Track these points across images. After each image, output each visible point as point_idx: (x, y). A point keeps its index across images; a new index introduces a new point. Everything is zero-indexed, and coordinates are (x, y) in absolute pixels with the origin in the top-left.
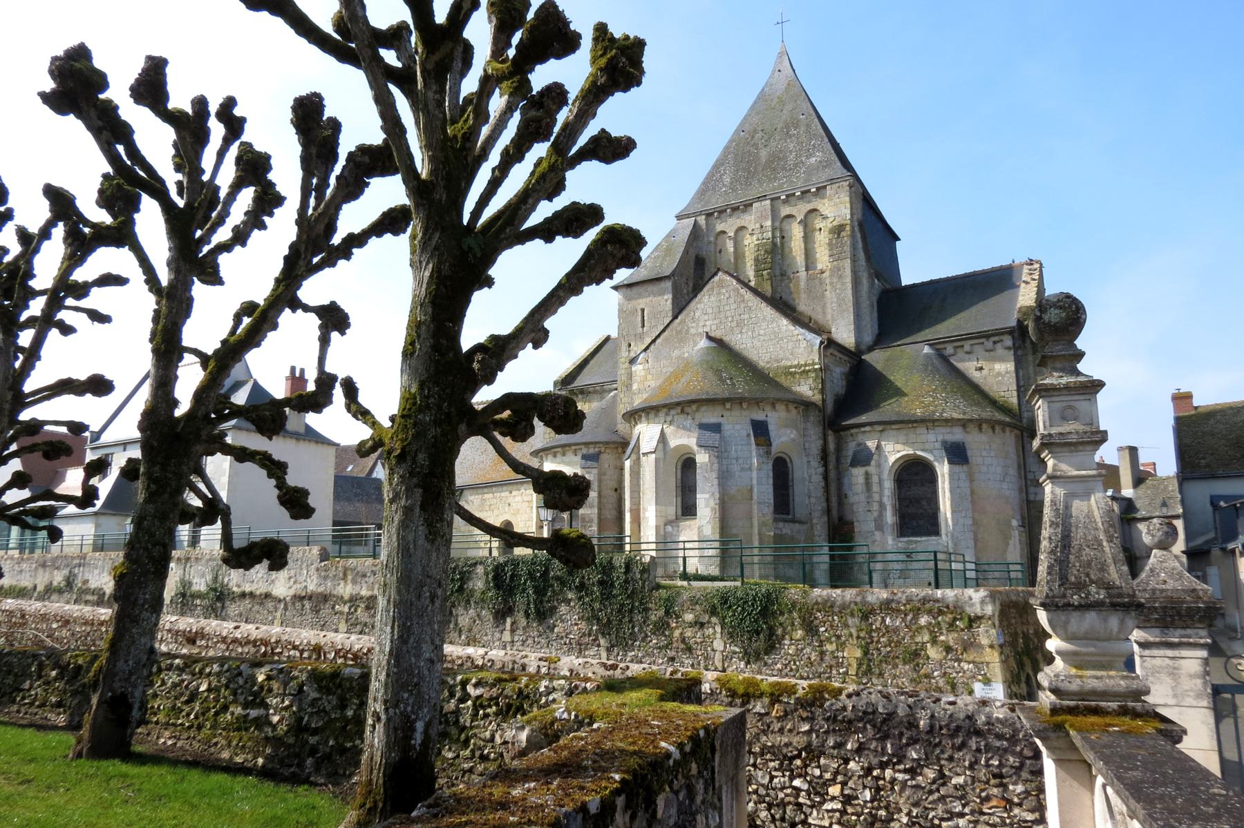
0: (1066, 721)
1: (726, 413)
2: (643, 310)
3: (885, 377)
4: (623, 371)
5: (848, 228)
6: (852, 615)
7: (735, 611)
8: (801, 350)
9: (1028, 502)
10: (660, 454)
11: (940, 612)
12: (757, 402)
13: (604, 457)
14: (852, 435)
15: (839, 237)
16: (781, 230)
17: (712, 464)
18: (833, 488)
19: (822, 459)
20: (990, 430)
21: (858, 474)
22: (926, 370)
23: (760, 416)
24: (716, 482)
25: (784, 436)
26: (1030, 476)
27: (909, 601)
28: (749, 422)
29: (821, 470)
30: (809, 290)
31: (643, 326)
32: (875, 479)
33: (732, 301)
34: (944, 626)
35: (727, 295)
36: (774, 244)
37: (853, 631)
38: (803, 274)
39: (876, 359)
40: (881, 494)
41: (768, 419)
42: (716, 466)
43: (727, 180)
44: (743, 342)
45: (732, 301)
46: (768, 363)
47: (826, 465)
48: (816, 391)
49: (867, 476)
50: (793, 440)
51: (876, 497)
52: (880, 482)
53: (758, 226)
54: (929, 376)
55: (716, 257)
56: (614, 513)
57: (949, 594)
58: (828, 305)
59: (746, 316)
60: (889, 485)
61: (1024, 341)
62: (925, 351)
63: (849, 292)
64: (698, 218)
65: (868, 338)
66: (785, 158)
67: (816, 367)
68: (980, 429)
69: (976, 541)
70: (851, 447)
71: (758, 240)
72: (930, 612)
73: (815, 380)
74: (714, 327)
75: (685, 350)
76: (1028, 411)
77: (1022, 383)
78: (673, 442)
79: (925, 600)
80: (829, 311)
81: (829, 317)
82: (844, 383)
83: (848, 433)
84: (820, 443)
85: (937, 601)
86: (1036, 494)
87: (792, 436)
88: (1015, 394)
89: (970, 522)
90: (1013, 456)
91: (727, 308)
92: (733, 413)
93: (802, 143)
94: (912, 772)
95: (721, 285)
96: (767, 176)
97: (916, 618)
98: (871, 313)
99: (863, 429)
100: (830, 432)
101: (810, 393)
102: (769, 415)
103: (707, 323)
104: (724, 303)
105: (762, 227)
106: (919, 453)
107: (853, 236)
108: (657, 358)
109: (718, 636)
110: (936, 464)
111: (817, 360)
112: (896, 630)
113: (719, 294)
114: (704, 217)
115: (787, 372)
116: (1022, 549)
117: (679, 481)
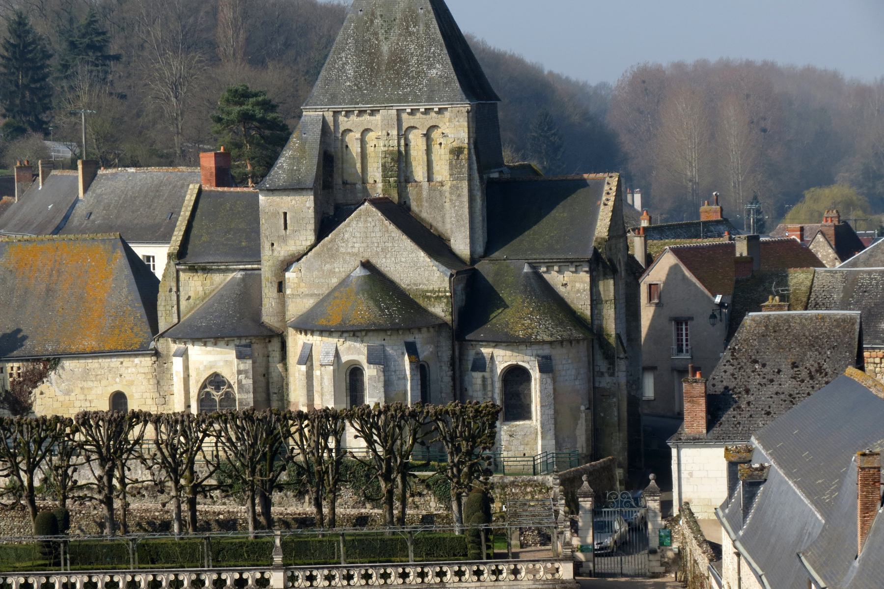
0: (266, 461)
1: (387, 338)
2: (285, 214)
3: (496, 294)
4: (267, 269)
5: (466, 152)
6: (497, 488)
7: (441, 488)
8: (435, 279)
9: (594, 388)
10: (336, 365)
11: (536, 486)
12: (409, 330)
13: (255, 346)
14: (472, 345)
15: (458, 158)
16: (406, 139)
17: (379, 377)
18: (458, 382)
19: (451, 365)
20: (569, 344)
21: (477, 376)
22: (526, 291)
23: (410, 339)
24: (382, 390)
25: (425, 351)
26: (597, 369)
27: (523, 481)
28: (403, 344)
29: (450, 373)
30: (430, 199)
31: (286, 228)
32: (489, 381)
33: (377, 229)
34: (537, 492)
35: (373, 224)
36: (399, 151)
37: (498, 495)
38: (425, 185)
39: (485, 268)
40: (493, 392)
41: (416, 340)
42: (382, 378)
43: (351, 73)
44: (388, 266)
45: (377, 229)
46: (408, 285)
47: (453, 370)
48: (447, 313)
49: (484, 379)
50: (432, 352)
51: (490, 394)
52: (493, 384)
53: (385, 133)
54: (527, 298)
55: (342, 152)
56: (264, 395)
57: (539, 478)
58: (447, 216)
59: (390, 245)
60: (498, 385)
61: (598, 265)
62: (525, 270)
63: (466, 210)
64: (326, 114)
65: (480, 250)
66: (405, 62)
67: (448, 294)
68: (562, 345)
69: (556, 424)
70: (471, 355)
71: (385, 146)
72: (531, 486)
73: (447, 304)
74: (362, 250)
75: (336, 265)
76: (598, 319)
77: (595, 298)
78: (344, 358)
79: (529, 481)
80: (448, 220)
81: (448, 226)
82: (464, 297)
83: (469, 343)
84: (450, 353)
85: (535, 481)
86: (600, 382)
87: (431, 350)
88: (589, 308)
89: (552, 412)
90: (585, 359)
91: (373, 235)
92: (392, 337)
93: (422, 47)
94: (532, 532)
95: (367, 213)
96: (390, 79)
97: (525, 489)
98: (483, 226)
99: (481, 343)
100: (456, 342)
101: (442, 314)
102: (417, 337)
103: (356, 245)
104: (370, 230)
105: (388, 134)
106: (520, 363)
107: (469, 158)
108: (310, 269)
109: (433, 500)
110: (531, 371)
111: (448, 289)
112: (517, 494)
113: (366, 221)
114: (331, 114)
115: (424, 295)
116: (587, 426)
117: (348, 385)
